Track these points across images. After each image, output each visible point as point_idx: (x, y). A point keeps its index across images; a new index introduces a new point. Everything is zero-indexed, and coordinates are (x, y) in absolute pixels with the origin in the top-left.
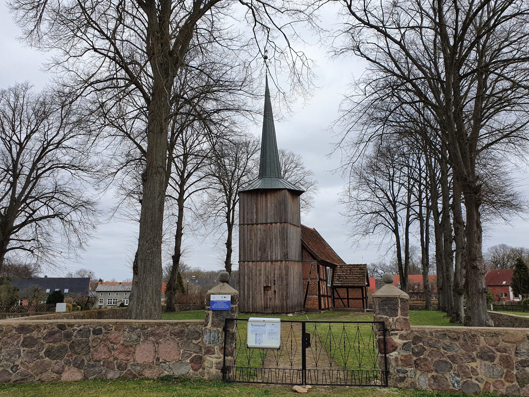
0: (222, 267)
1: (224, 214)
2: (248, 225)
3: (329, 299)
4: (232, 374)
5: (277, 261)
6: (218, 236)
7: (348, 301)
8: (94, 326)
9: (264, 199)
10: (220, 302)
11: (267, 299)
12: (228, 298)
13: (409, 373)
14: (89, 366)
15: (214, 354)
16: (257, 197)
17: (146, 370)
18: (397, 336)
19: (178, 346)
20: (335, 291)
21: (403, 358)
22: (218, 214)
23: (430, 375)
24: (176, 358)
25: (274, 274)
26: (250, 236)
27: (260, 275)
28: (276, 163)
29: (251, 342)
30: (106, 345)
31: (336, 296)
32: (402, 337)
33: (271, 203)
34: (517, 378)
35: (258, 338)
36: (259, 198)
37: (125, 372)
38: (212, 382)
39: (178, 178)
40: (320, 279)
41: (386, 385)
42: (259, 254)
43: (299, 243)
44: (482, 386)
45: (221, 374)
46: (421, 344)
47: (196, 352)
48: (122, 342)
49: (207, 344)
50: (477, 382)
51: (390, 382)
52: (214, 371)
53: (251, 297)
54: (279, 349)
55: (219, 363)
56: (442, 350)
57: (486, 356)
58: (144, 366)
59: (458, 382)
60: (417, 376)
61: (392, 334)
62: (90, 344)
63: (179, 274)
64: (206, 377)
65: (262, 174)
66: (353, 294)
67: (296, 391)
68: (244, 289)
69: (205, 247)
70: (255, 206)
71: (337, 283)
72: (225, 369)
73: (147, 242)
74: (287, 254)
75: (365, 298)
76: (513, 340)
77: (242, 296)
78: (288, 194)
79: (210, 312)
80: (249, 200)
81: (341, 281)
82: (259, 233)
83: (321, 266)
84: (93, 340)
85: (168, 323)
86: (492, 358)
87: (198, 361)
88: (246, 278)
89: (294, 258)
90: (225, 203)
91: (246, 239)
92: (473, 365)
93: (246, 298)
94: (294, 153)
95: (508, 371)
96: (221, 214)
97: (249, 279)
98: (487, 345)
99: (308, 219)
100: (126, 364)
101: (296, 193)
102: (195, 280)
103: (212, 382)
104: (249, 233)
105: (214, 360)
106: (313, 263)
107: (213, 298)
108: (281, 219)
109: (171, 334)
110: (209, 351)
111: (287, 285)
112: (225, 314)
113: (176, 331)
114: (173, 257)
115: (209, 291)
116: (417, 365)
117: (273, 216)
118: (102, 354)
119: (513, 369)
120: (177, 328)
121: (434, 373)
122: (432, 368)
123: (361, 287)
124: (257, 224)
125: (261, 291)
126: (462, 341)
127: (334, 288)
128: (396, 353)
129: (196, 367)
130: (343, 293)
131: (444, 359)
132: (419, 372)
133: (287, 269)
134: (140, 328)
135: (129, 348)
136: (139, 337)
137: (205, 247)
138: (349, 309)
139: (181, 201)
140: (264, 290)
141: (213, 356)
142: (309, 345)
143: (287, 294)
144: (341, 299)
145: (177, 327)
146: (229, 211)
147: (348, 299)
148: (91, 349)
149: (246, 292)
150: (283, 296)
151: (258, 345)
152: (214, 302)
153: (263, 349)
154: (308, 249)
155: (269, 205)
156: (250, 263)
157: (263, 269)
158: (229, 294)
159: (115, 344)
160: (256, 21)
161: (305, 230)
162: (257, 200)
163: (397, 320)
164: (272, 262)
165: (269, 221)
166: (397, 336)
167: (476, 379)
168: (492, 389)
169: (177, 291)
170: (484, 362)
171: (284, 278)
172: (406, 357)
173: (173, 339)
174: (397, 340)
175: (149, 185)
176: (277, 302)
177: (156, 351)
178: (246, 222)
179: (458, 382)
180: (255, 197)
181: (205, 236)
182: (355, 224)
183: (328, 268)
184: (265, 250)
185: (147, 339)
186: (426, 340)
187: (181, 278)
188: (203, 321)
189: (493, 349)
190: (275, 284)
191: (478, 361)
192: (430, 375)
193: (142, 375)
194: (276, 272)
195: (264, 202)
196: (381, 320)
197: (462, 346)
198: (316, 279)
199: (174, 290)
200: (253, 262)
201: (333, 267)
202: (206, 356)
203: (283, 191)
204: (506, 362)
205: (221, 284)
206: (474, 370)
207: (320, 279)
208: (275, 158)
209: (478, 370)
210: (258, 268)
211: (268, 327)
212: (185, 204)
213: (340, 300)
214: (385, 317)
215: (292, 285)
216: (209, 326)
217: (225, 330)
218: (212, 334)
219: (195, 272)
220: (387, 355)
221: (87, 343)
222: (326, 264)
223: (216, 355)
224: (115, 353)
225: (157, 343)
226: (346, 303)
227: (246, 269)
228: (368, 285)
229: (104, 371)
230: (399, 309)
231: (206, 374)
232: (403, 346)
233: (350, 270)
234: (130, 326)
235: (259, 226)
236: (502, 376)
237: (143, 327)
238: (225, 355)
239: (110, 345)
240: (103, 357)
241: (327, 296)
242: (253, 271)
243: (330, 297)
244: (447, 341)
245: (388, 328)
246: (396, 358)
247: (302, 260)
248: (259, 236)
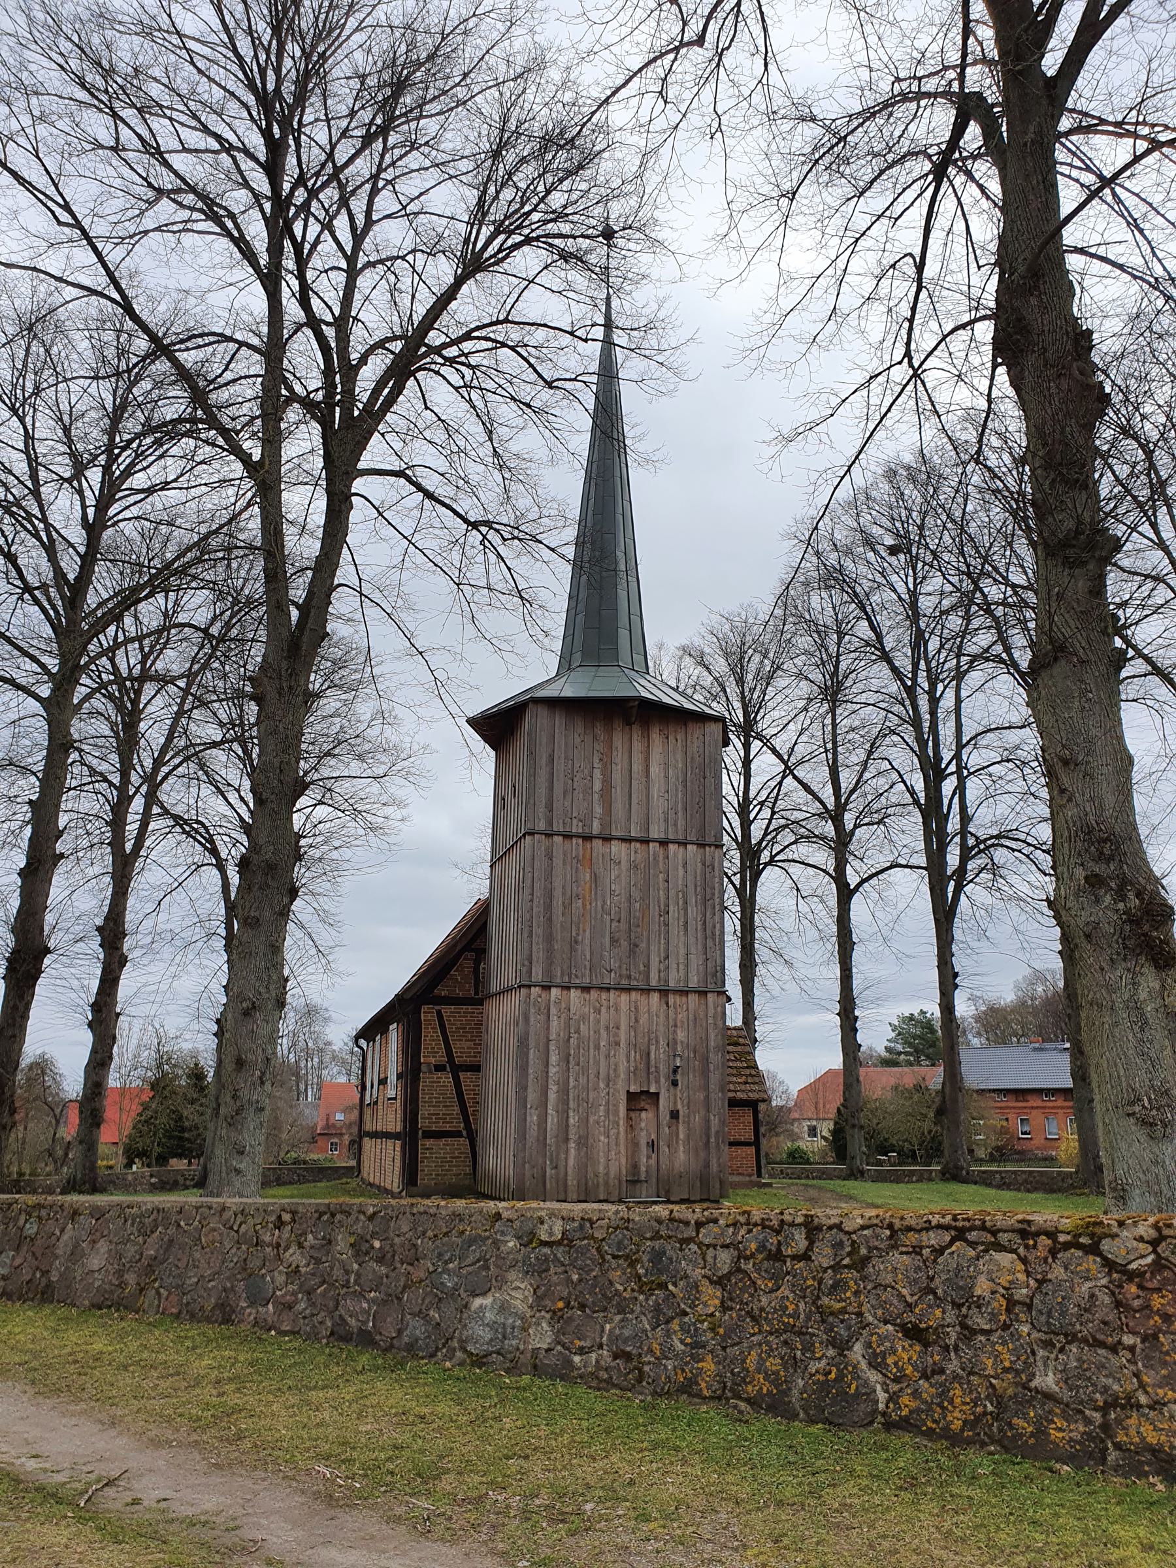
5: (684, 993)
16: (609, 731)
36: (689, 731)
88: (554, 1058)
125: (617, 1113)
155: (655, 770)
165: (655, 834)
195: (637, 758)
235: (615, 846)
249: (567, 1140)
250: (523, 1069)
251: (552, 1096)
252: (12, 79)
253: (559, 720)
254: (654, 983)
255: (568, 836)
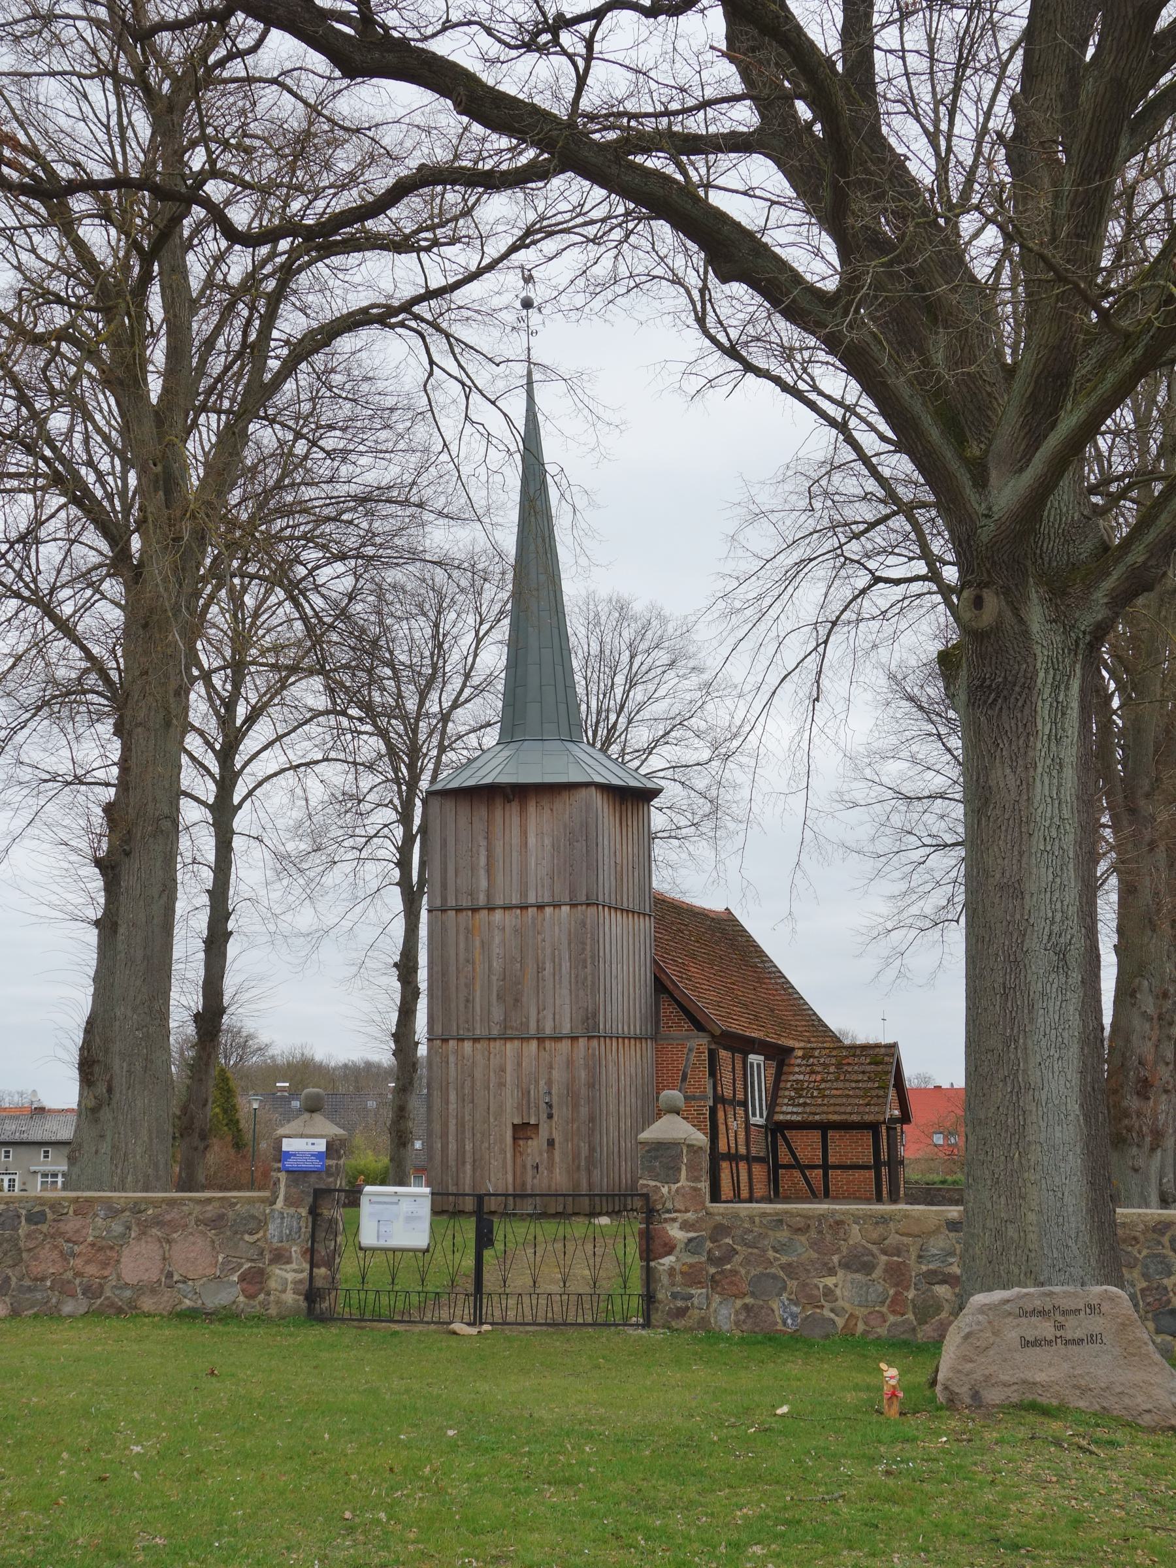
0: (383, 1054)
1: (389, 851)
2: (458, 911)
3: (757, 1169)
4: (327, 1304)
5: (558, 1039)
6: (367, 934)
7: (826, 1175)
8: (28, 1206)
9: (516, 820)
10: (303, 1154)
11: (524, 1167)
12: (321, 1146)
13: (696, 1301)
14: (20, 1288)
15: (289, 1262)
17: (144, 1299)
18: (677, 1225)
19: (214, 1248)
20: (780, 1141)
21: (685, 1269)
22: (364, 854)
23: (739, 1303)
24: (208, 1271)
25: (549, 1083)
26: (467, 950)
27: (502, 1085)
28: (561, 687)
29: (369, 1236)
30: (56, 1247)
31: (784, 1157)
32: (685, 1226)
33: (540, 835)
34: (914, 1306)
35: (382, 1229)
36: (498, 813)
37: (99, 1301)
38: (284, 1318)
39: (212, 727)
40: (719, 1099)
41: (647, 1324)
42: (497, 1014)
43: (645, 976)
44: (840, 1322)
45: (304, 1305)
46: (729, 1241)
47: (252, 1260)
48: (90, 1239)
49: (276, 1244)
50: (832, 1315)
51: (656, 1318)
52: (289, 1297)
53: (469, 1160)
54: (427, 1250)
55: (301, 1281)
56: (771, 1254)
57: (859, 1263)
58: (140, 1289)
59: (794, 1316)
60: (714, 1305)
61: (666, 1220)
62: (22, 1244)
63: (224, 1078)
64: (273, 1311)
65: (513, 725)
66: (844, 1148)
67: (455, 1333)
68: (445, 1135)
69: (315, 973)
70: (484, 843)
71: (788, 1112)
72: (312, 1295)
73: (134, 1010)
74: (595, 1015)
75: (888, 1164)
76: (915, 1230)
77: (438, 1157)
78: (598, 800)
79: (283, 1176)
80: (463, 821)
81: (805, 1104)
82: (497, 940)
83: (723, 1054)
84: (28, 1236)
85: (190, 1199)
86: (867, 1268)
87: (255, 1280)
88: (452, 1097)
89: (622, 1029)
90: (395, 809)
91: (453, 961)
92: (830, 1281)
93: (452, 1163)
94: (666, 612)
95: (897, 1294)
96: (381, 853)
97: (461, 1099)
98: (864, 1242)
99: (688, 874)
100: (101, 1286)
101: (634, 799)
102: (287, 1100)
103: (284, 1318)
104: (462, 938)
105: (290, 1276)
106: (693, 1043)
107: (288, 1145)
108: (572, 892)
109: (198, 1222)
110: (280, 1257)
111: (592, 1119)
112: (313, 1179)
113: (208, 1215)
114: (198, 1018)
115: (281, 1131)
116: (714, 1281)
117: (547, 881)
118: (47, 1263)
119: (907, 1288)
120: (211, 1211)
121: (748, 1300)
122: (745, 1287)
123: (874, 1127)
124: (491, 909)
126: (813, 1234)
127: (776, 1129)
128: (672, 1258)
129: (252, 1289)
130: (807, 1146)
131: (773, 1270)
132: (717, 1298)
133: (594, 1067)
134: (131, 1210)
135: (106, 1251)
136: (129, 1228)
137: (315, 973)
139: (223, 812)
141: (288, 1267)
142: (490, 1243)
143: (592, 1149)
144: (802, 1168)
145: (209, 1208)
146: (409, 839)
147: (826, 1167)
148: (25, 1255)
149: (452, 1146)
150: (576, 1156)
151: (382, 1243)
152: (288, 1155)
153: (394, 1250)
154: (676, 994)
155: (532, 840)
156: (467, 1045)
157: (509, 1069)
158: (322, 1137)
159: (75, 1243)
160: (432, 362)
161: (678, 923)
162: (489, 822)
163: (677, 1190)
165: (532, 899)
166: (677, 1225)
167: (832, 1310)
168: (861, 1327)
169: (215, 1141)
170: (850, 1276)
172: (691, 1266)
173: (201, 1232)
174: (676, 1233)
175: (137, 866)
176: (559, 1179)
177: (164, 1259)
178: (451, 902)
179: (794, 1316)
180: (483, 812)
181: (318, 936)
182: (903, 886)
183: (755, 1059)
184: (517, 1000)
185: (144, 1233)
186: (739, 1232)
187: (229, 1091)
188: (267, 1194)
189: (874, 1248)
190: (550, 1116)
191: (841, 1273)
192: (739, 1303)
193: (136, 1308)
194: (555, 1074)
196: (645, 1191)
197: (814, 1244)
198: (705, 1098)
199: (203, 1137)
200: (476, 1040)
201: (779, 1055)
202: (273, 1267)
203: (583, 792)
204: (897, 1274)
205: (307, 1116)
206: (829, 1293)
207: (719, 1099)
208: (559, 668)
209: (838, 1292)
210: (494, 1062)
211: (406, 1206)
212: (241, 822)
213: (797, 1173)
214: (653, 1183)
215: (612, 1121)
216: (280, 1204)
217: (314, 1212)
218: (284, 1219)
219: (289, 1065)
220: (652, 1264)
221: (14, 1241)
222: (742, 1045)
223: (294, 1266)
224: (77, 1263)
225: (168, 1242)
226: (818, 1184)
227: (452, 1066)
228: (905, 1118)
229: (54, 1300)
230: (684, 1168)
231: (272, 1306)
232: (687, 1245)
233: (839, 1066)
234: (107, 1203)
235: (498, 915)
236: (883, 1302)
237: (136, 1208)
238: (313, 1265)
239: (66, 1246)
240: (51, 1271)
241: (749, 1159)
242: (478, 1074)
244: (783, 1235)
245: (659, 1207)
246: (672, 1269)
247: (655, 1035)
248: (496, 950)
249: (464, 1163)
250: (745, 1075)
251: (452, 1128)
252: (226, 74)
253: (449, 805)
254: (533, 1030)
255: (458, 910)
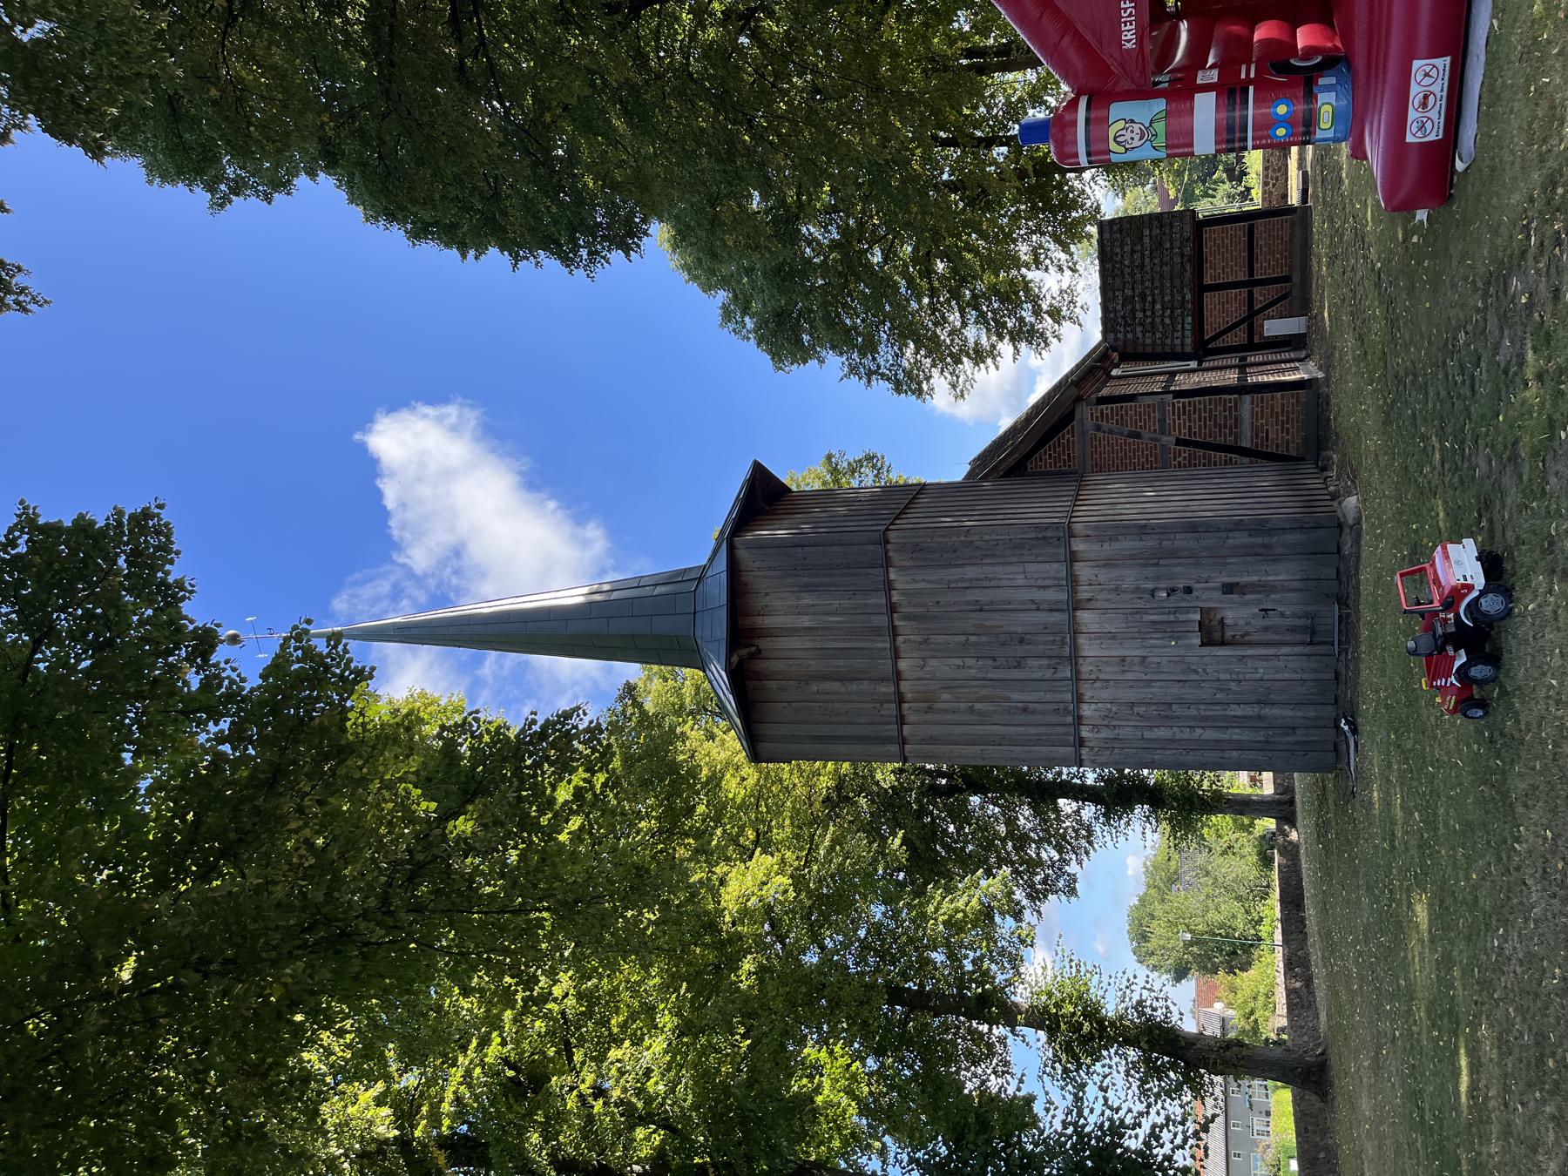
9: (783, 643)
11: (1266, 629)
20: (1218, 343)
31: (1239, 336)
70: (814, 687)
88: (1162, 733)
101: (763, 496)
104: (938, 717)
106: (1089, 424)
124: (898, 676)
138: (1296, 278)
140: (1223, 643)
154: (1024, 450)
164: (1076, 606)
165: (883, 620)
171: (1160, 546)
198: (1162, 405)
200: (1079, 699)
203: (742, 553)
210: (1110, 672)
226: (1273, 291)
242: (1131, 695)
243: (1243, 359)
247: (1074, 476)
